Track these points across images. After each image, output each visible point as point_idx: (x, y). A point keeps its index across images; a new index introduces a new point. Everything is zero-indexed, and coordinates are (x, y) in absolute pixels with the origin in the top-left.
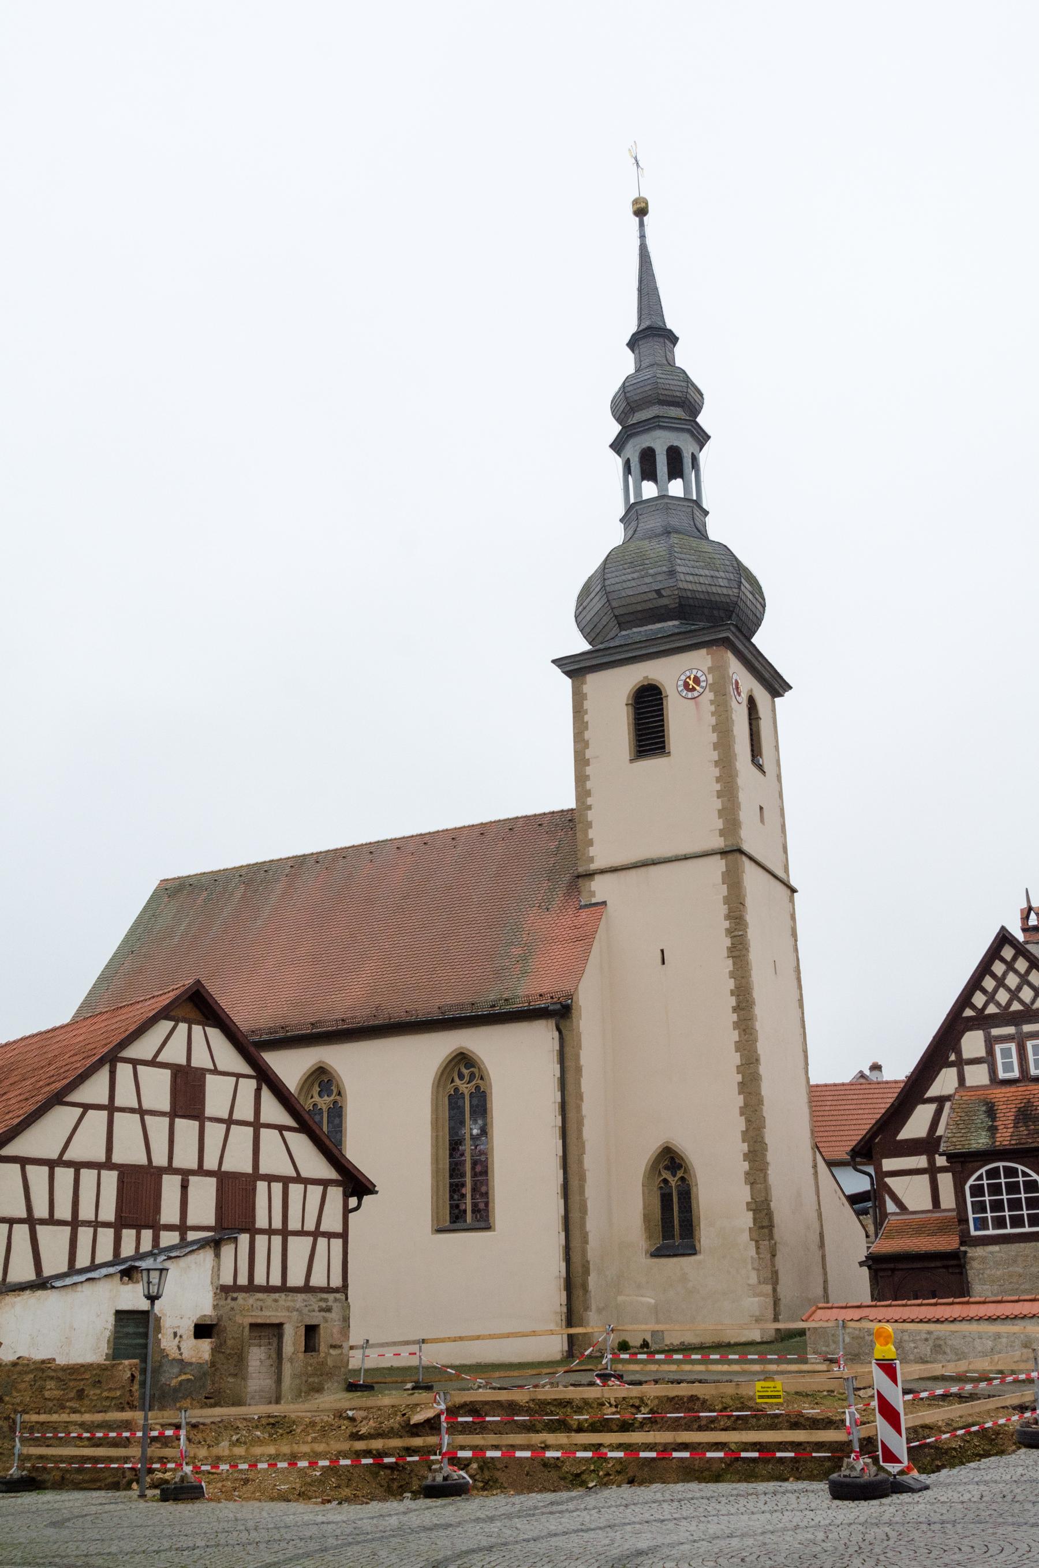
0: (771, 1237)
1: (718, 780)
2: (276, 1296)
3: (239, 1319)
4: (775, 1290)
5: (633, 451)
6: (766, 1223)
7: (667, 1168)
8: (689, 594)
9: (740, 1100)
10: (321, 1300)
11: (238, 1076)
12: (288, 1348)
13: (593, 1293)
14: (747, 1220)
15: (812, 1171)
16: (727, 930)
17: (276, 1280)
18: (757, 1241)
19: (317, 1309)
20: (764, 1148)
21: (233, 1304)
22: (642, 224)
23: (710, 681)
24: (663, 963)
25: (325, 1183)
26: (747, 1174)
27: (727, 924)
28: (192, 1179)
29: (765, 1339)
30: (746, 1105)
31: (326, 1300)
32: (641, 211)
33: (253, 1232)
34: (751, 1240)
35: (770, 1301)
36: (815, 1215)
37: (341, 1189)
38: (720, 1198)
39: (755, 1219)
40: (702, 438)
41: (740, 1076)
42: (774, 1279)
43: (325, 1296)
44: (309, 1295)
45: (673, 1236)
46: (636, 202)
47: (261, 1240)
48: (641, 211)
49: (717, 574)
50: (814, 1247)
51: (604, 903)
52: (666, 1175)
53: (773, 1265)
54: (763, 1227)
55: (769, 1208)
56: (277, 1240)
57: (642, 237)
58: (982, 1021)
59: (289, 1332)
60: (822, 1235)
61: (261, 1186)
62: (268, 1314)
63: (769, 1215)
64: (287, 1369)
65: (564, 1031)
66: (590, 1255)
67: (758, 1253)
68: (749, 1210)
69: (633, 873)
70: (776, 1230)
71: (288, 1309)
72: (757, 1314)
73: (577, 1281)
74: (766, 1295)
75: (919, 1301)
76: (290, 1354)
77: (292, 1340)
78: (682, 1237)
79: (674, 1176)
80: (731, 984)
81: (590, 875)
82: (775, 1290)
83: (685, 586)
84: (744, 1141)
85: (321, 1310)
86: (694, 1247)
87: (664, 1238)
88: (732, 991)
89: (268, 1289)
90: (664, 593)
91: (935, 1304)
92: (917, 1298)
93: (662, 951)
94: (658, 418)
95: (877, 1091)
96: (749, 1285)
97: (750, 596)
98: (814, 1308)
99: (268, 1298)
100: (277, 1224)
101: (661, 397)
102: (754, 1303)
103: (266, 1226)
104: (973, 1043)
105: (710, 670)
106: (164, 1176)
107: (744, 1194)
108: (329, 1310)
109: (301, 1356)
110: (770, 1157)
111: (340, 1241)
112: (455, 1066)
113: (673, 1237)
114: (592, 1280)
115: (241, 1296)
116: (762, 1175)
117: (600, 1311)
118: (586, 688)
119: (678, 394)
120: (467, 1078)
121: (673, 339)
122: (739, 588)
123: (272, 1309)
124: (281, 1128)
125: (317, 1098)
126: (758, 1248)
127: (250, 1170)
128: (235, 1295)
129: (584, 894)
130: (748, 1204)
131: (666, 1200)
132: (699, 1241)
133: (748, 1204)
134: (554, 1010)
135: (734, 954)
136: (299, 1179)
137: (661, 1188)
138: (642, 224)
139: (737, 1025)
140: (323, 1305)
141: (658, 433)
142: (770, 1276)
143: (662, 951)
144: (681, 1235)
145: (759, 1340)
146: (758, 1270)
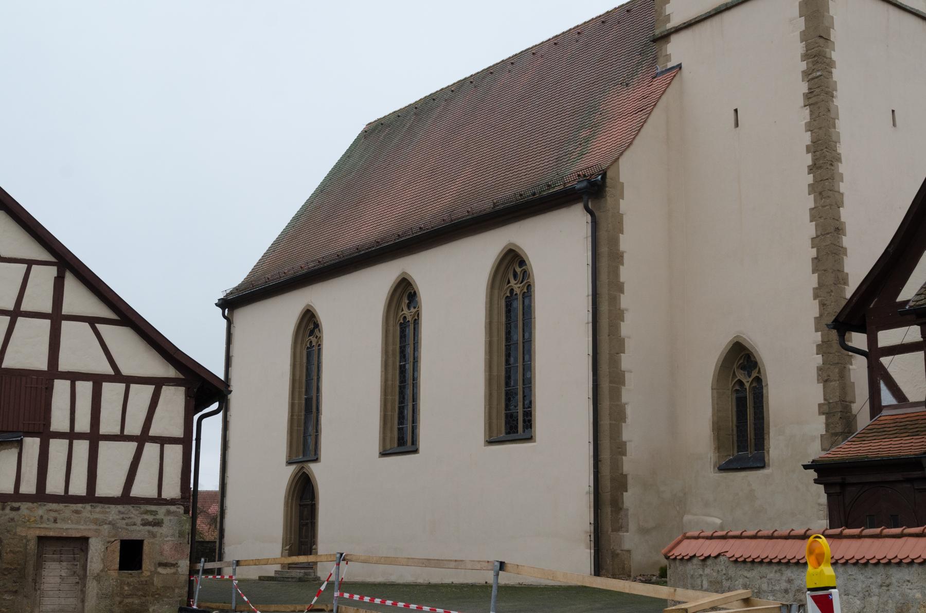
2: (79, 506)
3: (21, 531)
7: (743, 367)
10: (146, 512)
11: (30, 263)
12: (95, 562)
13: (631, 512)
16: (803, 72)
17: (78, 487)
19: (139, 521)
21: (13, 514)
24: (737, 125)
25: (158, 383)
26: (820, 369)
27: (803, 66)
28: (106, 385)
31: (154, 513)
33: (46, 435)
37: (183, 389)
39: (827, 425)
41: (815, 250)
43: (153, 508)
44: (130, 507)
47: (58, 448)
51: (679, 67)
52: (741, 375)
56: (82, 448)
59: (96, 547)
61: (61, 388)
62: (65, 526)
64: (92, 588)
65: (597, 214)
68: (821, 413)
69: (707, 25)
71: (96, 521)
73: (606, 496)
75: (898, 530)
76: (97, 571)
77: (100, 555)
81: (665, 37)
84: (817, 331)
85: (145, 523)
88: (807, 147)
89: (66, 499)
91: (859, 537)
92: (896, 526)
96: (819, 504)
98: (680, 537)
99: (67, 510)
100: (83, 424)
103: (66, 428)
106: (104, 384)
108: (158, 523)
109: (114, 574)
111: (178, 449)
112: (507, 268)
114: (629, 498)
115: (25, 507)
117: (643, 531)
120: (520, 277)
123: (70, 523)
124: (92, 321)
125: (406, 311)
127: (44, 367)
128: (16, 505)
129: (661, 60)
130: (820, 405)
131: (741, 404)
133: (820, 405)
134: (580, 189)
135: (811, 101)
136: (117, 377)
137: (737, 391)
140: (150, 518)
143: (736, 111)
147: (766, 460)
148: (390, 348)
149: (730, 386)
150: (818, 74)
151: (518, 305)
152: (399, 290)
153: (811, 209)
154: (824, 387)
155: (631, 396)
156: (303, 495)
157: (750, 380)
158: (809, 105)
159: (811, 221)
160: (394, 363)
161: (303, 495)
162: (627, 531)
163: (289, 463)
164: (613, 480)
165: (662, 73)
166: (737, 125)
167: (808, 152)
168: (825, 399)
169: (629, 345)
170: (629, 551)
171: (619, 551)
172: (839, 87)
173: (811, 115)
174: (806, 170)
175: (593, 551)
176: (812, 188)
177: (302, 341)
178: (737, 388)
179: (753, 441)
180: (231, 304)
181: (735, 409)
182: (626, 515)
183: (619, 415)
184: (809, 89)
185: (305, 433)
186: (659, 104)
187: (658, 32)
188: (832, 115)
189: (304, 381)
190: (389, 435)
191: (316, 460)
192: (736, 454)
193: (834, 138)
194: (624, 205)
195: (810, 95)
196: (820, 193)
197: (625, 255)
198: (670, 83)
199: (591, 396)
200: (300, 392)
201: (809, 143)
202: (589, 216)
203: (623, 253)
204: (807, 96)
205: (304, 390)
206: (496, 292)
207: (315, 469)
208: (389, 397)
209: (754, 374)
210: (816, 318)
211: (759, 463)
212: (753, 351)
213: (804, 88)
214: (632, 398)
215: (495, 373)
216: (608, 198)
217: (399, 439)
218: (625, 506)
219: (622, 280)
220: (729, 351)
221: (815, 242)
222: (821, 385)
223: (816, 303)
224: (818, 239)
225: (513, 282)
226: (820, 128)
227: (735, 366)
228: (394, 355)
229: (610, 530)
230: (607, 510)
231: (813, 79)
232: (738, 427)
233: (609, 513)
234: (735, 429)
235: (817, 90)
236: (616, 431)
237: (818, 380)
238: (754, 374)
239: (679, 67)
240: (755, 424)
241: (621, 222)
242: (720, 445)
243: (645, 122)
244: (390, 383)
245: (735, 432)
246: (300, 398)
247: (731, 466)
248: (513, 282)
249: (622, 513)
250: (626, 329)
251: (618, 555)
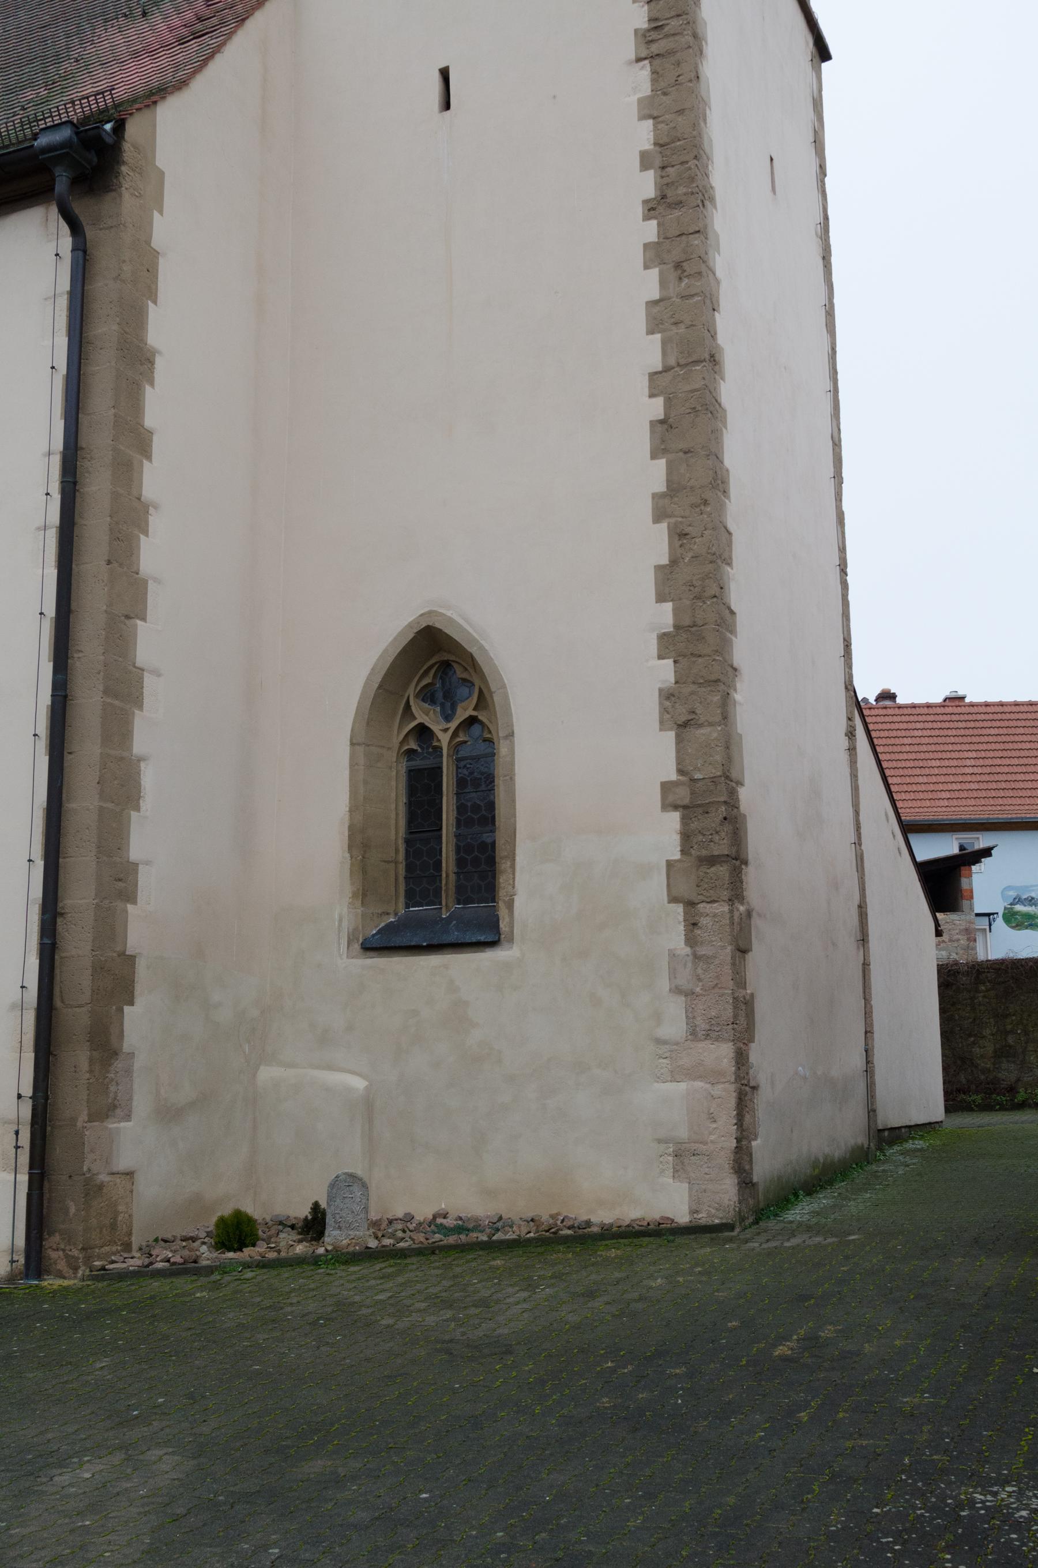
0: (736, 892)
4: (741, 1059)
6: (722, 847)
7: (427, 695)
9: (655, 475)
13: (138, 1064)
14: (663, 836)
15: (844, 743)
18: (690, 904)
20: (725, 621)
24: (447, 105)
26: (667, 696)
29: (703, 1218)
30: (674, 488)
34: (673, 899)
35: (726, 1093)
36: (850, 855)
38: (583, 775)
39: (686, 836)
41: (660, 401)
42: (741, 1022)
45: (438, 893)
50: (847, 942)
52: (424, 715)
53: (741, 982)
54: (712, 861)
55: (732, 802)
60: (862, 908)
63: (734, 823)
65: (90, 233)
66: (139, 933)
67: (691, 941)
68: (668, 805)
70: (751, 875)
72: (683, 1133)
73: (76, 1016)
74: (713, 1076)
78: (463, 896)
79: (448, 718)
80: (644, 135)
82: (741, 1059)
84: (661, 598)
86: (493, 925)
87: (411, 899)
93: (445, 74)
95: (898, 719)
96: (659, 1042)
102: (675, 1100)
107: (658, 756)
110: (743, 651)
113: (433, 896)
114: (139, 1023)
116: (716, 698)
117: (169, 1114)
126: (692, 925)
130: (666, 787)
132: (510, 905)
133: (666, 787)
135: (655, 48)
137: (410, 753)
139: (654, 254)
142: (729, 1013)
143: (445, 74)
144: (460, 889)
145: (683, 1218)
146: (689, 994)
147: (503, 926)
149: (396, 746)
153: (651, 304)
154: (679, 740)
155: (158, 736)
157: (453, 725)
158: (651, 57)
159: (650, 332)
162: (128, 1117)
164: (99, 969)
168: (680, 772)
169: (157, 600)
170: (130, 1174)
171: (103, 1177)
173: (654, 81)
174: (639, 211)
175: (24, 1178)
178: (413, 745)
179: (453, 877)
182: (129, 1072)
184: (651, 20)
192: (402, 911)
195: (654, 35)
196: (678, 266)
199: (43, 728)
202: (67, 242)
209: (463, 713)
210: (658, 568)
211: (484, 932)
212: (473, 650)
214: (165, 738)
216: (126, 195)
218: (126, 1047)
220: (404, 651)
221: (656, 383)
222: (671, 735)
223: (663, 528)
224: (669, 376)
229: (84, 1116)
230: (76, 1059)
232: (408, 842)
233: (84, 1065)
235: (674, 23)
237: (661, 722)
238: (463, 713)
240: (457, 836)
241: (152, 270)
242: (366, 889)
245: (401, 856)
247: (398, 941)
249: (119, 1065)
250: (153, 554)
251: (101, 1187)
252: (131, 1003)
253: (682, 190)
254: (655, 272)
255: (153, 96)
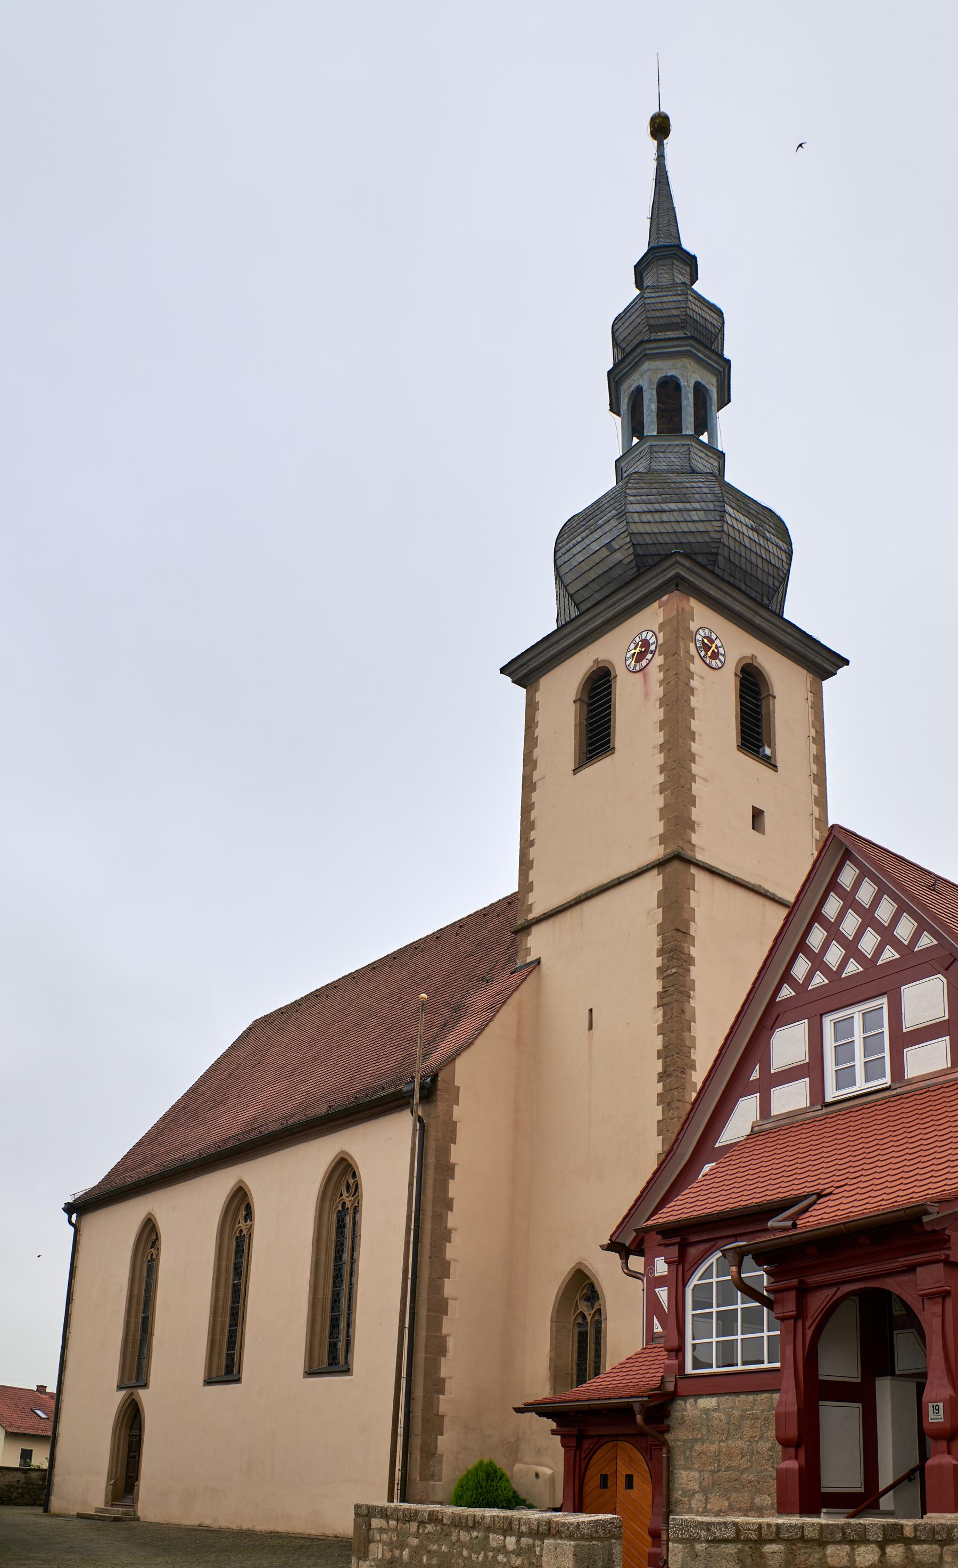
1: (662, 769)
5: (647, 377)
8: (648, 540)
16: (658, 969)
22: (660, 147)
23: (660, 641)
24: (591, 1027)
27: (658, 962)
32: (660, 127)
40: (723, 370)
46: (653, 119)
48: (660, 127)
49: (688, 506)
51: (538, 962)
52: (584, 1307)
57: (661, 157)
58: (813, 1007)
81: (526, 928)
83: (641, 528)
88: (659, 1051)
90: (615, 545)
94: (669, 351)
97: (755, 536)
101: (652, 322)
104: (788, 1045)
105: (662, 627)
118: (539, 697)
119: (674, 312)
121: (691, 261)
122: (722, 519)
129: (521, 954)
135: (665, 1001)
137: (579, 1324)
138: (660, 147)
141: (687, 361)
143: (591, 1010)
148: (224, 1264)
149: (572, 1319)
150: (674, 970)
151: (348, 1220)
152: (236, 1201)
153: (659, 1122)
156: (131, 1421)
157: (592, 1312)
158: (663, 1005)
159: (658, 1135)
160: (226, 1281)
161: (131, 1421)
163: (120, 1388)
165: (522, 968)
166: (591, 1027)
167: (659, 1058)
172: (697, 985)
173: (664, 1016)
176: (661, 1099)
177: (144, 1252)
178: (580, 1321)
180: (79, 1209)
181: (576, 1345)
183: (439, 1348)
184: (663, 987)
185: (139, 1356)
186: (509, 1001)
187: (520, 922)
188: (687, 1017)
189: (142, 1298)
190: (216, 1360)
191: (145, 1386)
193: (687, 1043)
194: (457, 1112)
195: (664, 995)
196: (669, 1104)
197: (457, 1169)
198: (525, 979)
200: (137, 1309)
201: (660, 1048)
203: (454, 1165)
204: (661, 996)
205: (142, 1307)
206: (327, 1205)
207: (144, 1395)
208: (219, 1319)
213: (658, 986)
215: (320, 1296)
216: (439, 1103)
217: (227, 1366)
218: (439, 1452)
219: (451, 1195)
225: (345, 1194)
226: (672, 1031)
227: (578, 1297)
228: (227, 1271)
231: (667, 976)
234: (575, 1367)
236: (433, 1367)
238: (596, 1308)
239: (538, 962)
243: (491, 1020)
244: (221, 1303)
245: (575, 1371)
246: (137, 1316)
248: (345, 1194)
252: (442, 1435)
253: (672, 1069)
254: (661, 1107)
255: (451, 1060)
